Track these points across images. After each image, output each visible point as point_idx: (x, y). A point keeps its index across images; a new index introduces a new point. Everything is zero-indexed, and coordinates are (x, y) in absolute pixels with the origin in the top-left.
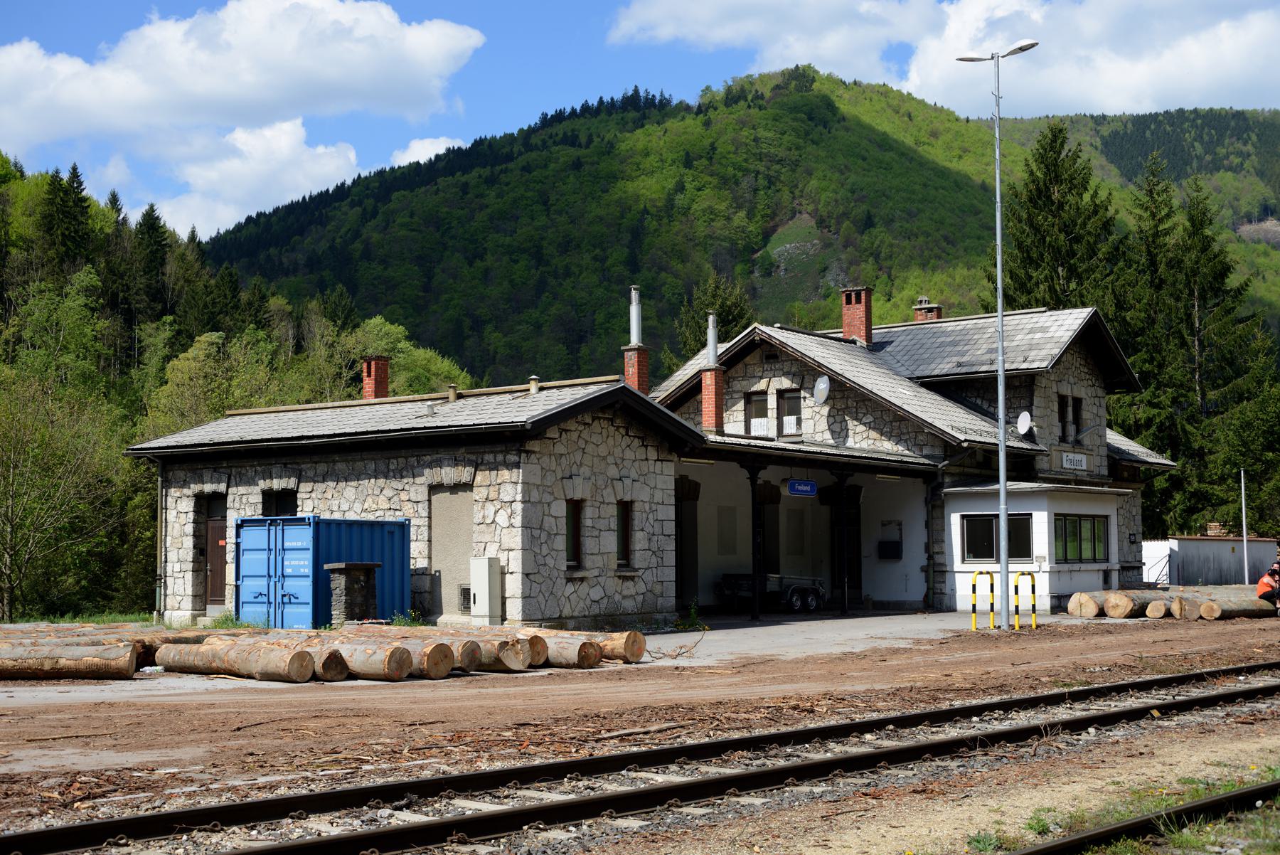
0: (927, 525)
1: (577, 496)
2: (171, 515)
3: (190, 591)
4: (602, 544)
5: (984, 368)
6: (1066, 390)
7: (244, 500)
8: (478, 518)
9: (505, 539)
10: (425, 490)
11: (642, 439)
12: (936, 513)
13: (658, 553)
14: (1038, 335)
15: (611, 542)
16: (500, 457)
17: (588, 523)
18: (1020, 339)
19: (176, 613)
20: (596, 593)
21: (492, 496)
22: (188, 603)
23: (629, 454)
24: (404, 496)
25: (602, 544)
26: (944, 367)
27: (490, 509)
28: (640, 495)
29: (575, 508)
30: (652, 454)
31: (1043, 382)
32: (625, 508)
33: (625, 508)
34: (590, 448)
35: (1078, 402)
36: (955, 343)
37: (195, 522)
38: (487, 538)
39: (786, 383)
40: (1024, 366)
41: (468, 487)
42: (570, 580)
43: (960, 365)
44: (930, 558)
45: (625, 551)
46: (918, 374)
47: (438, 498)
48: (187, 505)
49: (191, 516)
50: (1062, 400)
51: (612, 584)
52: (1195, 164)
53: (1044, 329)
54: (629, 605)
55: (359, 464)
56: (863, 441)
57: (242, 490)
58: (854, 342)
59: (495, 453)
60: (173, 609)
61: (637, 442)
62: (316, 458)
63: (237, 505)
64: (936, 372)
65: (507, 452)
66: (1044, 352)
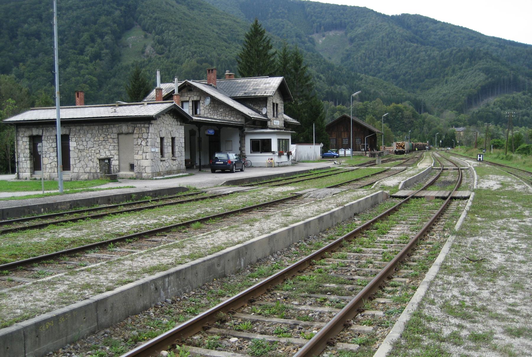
0: (240, 142)
1: (163, 136)
2: (20, 143)
3: (29, 166)
4: (168, 150)
5: (253, 95)
6: (274, 102)
7: (49, 137)
8: (135, 143)
9: (145, 149)
10: (116, 135)
11: (177, 119)
12: (243, 138)
13: (181, 152)
14: (268, 85)
15: (170, 149)
16: (142, 125)
17: (165, 144)
18: (262, 86)
19: (24, 174)
20: (167, 165)
21: (140, 136)
22: (28, 170)
23: (174, 123)
24: (109, 137)
25: (168, 150)
26: (240, 94)
27: (140, 141)
28: (176, 135)
29: (162, 139)
30: (179, 123)
31: (269, 99)
32: (173, 139)
33: (173, 139)
34: (165, 122)
35: (277, 104)
36: (243, 86)
37: (29, 145)
38: (139, 149)
39: (195, 98)
40: (265, 95)
41: (132, 133)
42: (161, 161)
43: (245, 93)
44: (241, 152)
45: (173, 152)
46: (232, 96)
47: (120, 136)
48: (26, 140)
49: (28, 143)
50: (273, 104)
51: (171, 162)
52: (269, 15)
53: (269, 83)
54: (175, 168)
55: (92, 127)
56: (217, 117)
57: (48, 134)
58: (211, 85)
59: (141, 124)
60: (23, 172)
61: (175, 120)
62: (76, 125)
63: (46, 139)
64: (238, 96)
65: (145, 124)
66: (270, 90)
